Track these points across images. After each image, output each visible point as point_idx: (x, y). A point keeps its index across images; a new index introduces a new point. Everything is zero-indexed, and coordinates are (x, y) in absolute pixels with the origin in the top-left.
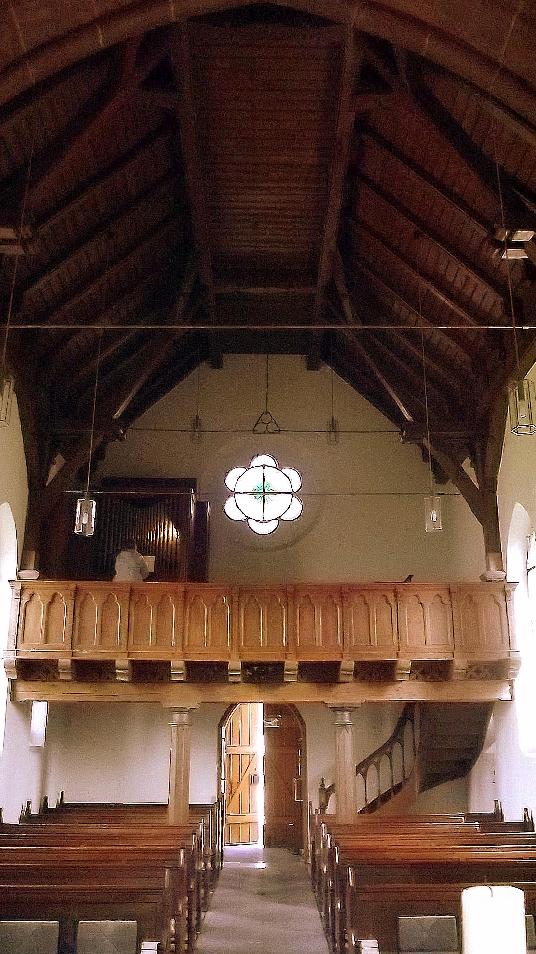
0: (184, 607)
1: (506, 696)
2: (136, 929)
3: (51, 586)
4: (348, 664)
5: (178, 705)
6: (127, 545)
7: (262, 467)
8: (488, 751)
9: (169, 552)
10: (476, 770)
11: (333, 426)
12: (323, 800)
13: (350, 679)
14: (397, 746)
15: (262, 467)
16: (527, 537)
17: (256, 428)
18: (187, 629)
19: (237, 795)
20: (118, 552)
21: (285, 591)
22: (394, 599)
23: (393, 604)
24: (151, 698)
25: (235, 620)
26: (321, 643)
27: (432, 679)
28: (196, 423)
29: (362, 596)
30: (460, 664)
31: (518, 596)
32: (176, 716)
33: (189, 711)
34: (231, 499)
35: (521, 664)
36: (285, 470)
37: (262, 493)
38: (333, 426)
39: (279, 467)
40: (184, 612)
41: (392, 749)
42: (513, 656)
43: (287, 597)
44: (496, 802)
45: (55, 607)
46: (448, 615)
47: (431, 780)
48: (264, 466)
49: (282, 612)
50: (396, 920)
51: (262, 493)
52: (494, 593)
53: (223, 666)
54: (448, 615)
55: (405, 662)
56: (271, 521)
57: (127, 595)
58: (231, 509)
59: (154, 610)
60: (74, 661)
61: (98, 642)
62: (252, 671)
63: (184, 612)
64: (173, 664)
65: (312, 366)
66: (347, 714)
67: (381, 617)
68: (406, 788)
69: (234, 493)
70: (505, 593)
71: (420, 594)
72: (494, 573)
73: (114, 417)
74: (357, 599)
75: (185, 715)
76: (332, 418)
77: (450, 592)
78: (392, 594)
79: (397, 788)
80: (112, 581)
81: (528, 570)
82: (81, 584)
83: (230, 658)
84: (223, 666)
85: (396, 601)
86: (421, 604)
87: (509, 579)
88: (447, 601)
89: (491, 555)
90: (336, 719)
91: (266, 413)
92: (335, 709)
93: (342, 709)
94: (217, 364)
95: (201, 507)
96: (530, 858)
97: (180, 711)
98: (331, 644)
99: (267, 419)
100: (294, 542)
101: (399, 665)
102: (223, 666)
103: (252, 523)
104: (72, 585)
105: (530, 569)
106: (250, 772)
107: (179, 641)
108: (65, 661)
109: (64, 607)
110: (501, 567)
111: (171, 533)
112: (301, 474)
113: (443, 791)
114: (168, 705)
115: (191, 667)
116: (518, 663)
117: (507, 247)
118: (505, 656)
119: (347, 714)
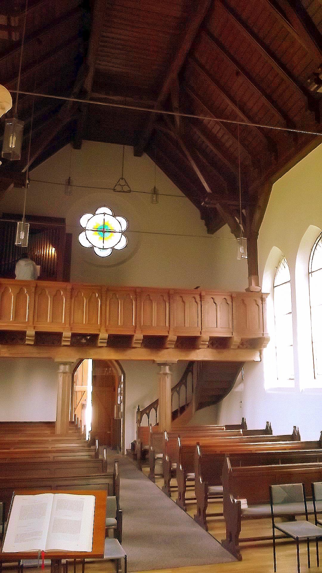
0: (71, 298)
1: (257, 359)
2: (116, 499)
4: (139, 336)
5: (64, 360)
7: (103, 215)
8: (238, 388)
9: (49, 264)
10: (225, 401)
11: (155, 192)
12: (139, 418)
13: (139, 346)
14: (183, 387)
15: (103, 215)
16: (276, 267)
18: (73, 312)
20: (17, 261)
21: (135, 292)
22: (199, 299)
23: (199, 302)
24: (46, 355)
25: (103, 307)
26: (156, 324)
27: (217, 348)
28: (69, 182)
29: (181, 297)
30: (237, 339)
31: (269, 300)
32: (62, 367)
34: (83, 234)
35: (270, 340)
36: (118, 218)
37: (103, 231)
38: (155, 192)
39: (114, 216)
40: (71, 301)
41: (180, 389)
42: (265, 336)
43: (136, 295)
44: (243, 419)
46: (230, 311)
47: (200, 406)
48: (104, 214)
49: (133, 304)
50: (313, 486)
51: (103, 231)
52: (256, 299)
53: (60, 335)
54: (230, 311)
55: (172, 337)
56: (88, 240)
57: (33, 289)
58: (82, 240)
59: (51, 300)
60: (36, 333)
61: (13, 319)
62: (86, 339)
63: (71, 301)
64: (101, 336)
65: (137, 154)
66: (167, 367)
67: (192, 309)
68: (187, 410)
69: (84, 230)
70: (263, 300)
71: (183, 295)
72: (254, 287)
73: (22, 172)
74: (178, 298)
75: (67, 367)
76: (155, 188)
78: (199, 297)
79: (182, 409)
80: (15, 279)
81: (274, 287)
83: (100, 331)
84: (60, 335)
85: (201, 301)
86: (215, 303)
87: (263, 291)
88: (230, 303)
89: (253, 277)
90: (160, 370)
92: (160, 365)
93: (165, 364)
94: (77, 146)
96: (290, 449)
97: (65, 364)
98: (162, 325)
100: (119, 264)
101: (202, 339)
102: (59, 335)
103: (96, 250)
105: (275, 287)
106: (82, 402)
107: (68, 319)
110: (258, 284)
111: (51, 251)
112: (127, 221)
113: (205, 411)
114: (57, 360)
115: (39, 335)
116: (268, 340)
117: (21, 96)
118: (261, 336)
119: (167, 368)
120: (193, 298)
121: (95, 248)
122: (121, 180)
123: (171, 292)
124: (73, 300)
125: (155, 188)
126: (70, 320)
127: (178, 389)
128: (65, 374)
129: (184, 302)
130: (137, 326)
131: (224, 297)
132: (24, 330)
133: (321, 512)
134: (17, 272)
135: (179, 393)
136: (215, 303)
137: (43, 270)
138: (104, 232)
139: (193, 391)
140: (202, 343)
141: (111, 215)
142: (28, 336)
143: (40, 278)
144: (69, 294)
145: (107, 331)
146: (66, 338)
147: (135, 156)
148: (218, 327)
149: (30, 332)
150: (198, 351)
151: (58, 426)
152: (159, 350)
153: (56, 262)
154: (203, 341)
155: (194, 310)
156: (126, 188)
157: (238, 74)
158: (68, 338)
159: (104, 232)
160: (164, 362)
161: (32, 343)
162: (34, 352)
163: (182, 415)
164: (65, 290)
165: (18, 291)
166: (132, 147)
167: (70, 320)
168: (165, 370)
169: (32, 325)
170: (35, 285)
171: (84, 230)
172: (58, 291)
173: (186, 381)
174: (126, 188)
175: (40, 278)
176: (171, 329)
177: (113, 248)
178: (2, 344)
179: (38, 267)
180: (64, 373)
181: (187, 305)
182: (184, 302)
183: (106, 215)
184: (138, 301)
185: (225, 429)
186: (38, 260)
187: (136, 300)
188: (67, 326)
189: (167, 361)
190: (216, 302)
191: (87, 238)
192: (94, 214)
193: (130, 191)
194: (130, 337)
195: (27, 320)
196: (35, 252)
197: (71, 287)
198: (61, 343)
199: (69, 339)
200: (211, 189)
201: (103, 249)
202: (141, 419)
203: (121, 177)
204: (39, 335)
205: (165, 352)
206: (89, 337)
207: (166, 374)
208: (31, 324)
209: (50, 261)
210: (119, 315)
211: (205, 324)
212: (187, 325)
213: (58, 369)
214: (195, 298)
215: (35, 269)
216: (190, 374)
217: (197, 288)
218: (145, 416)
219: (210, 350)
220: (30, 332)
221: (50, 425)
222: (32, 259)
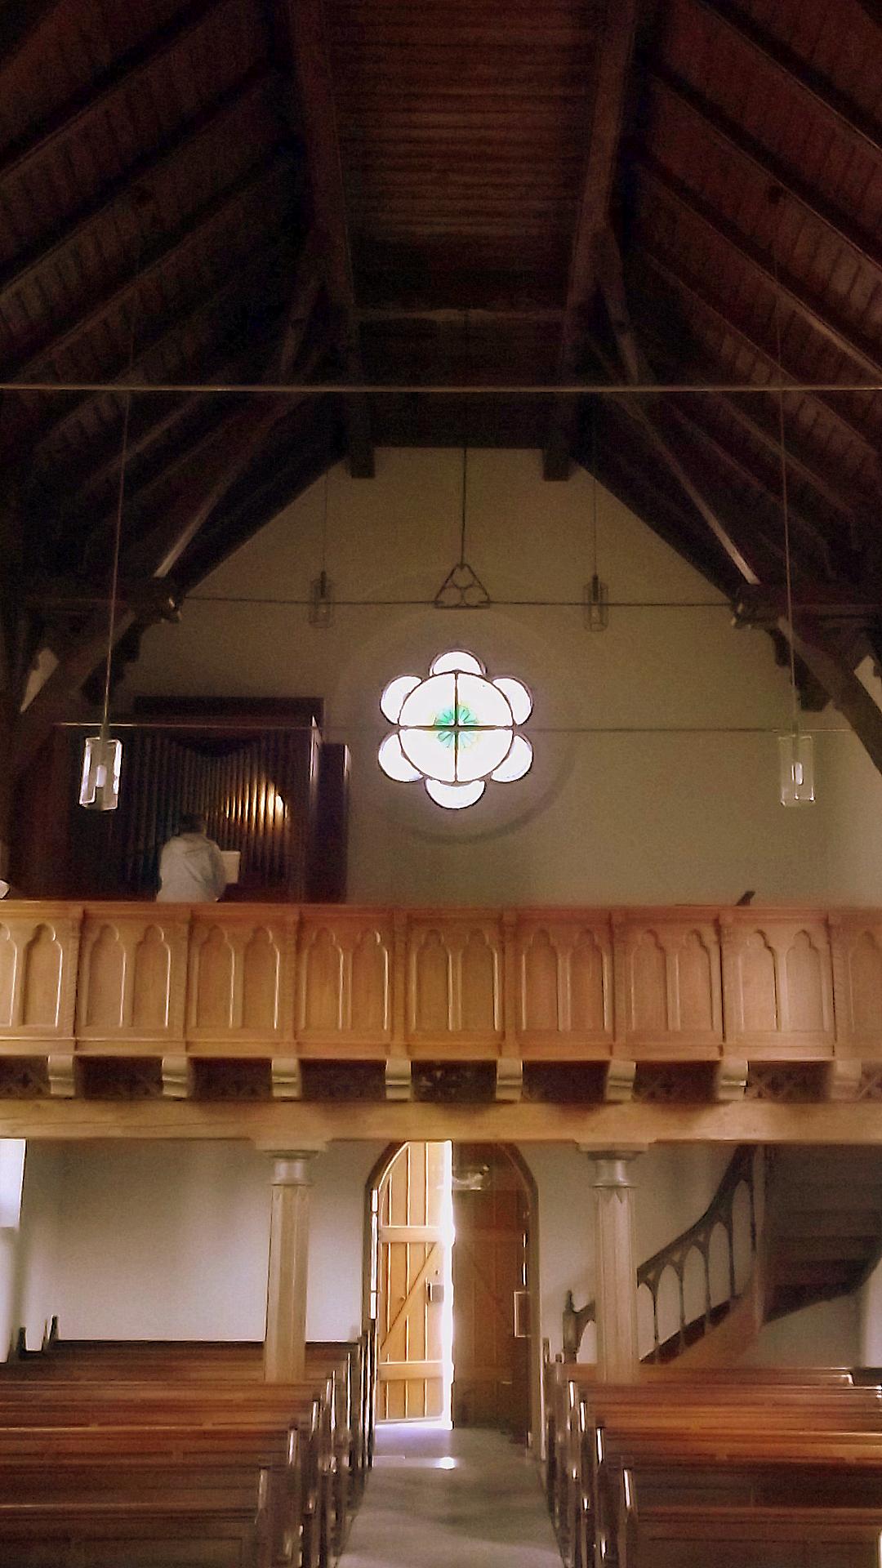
3: (32, 910)
4: (622, 1067)
5: (287, 1145)
6: (188, 825)
11: (596, 589)
12: (571, 1334)
13: (628, 1095)
14: (718, 1232)
17: (442, 598)
19: (400, 1324)
20: (165, 840)
21: (500, 921)
22: (714, 938)
24: (231, 1132)
27: (789, 1099)
28: (322, 587)
29: (650, 931)
30: (846, 1068)
32: (282, 1169)
33: (308, 1155)
38: (596, 589)
39: (488, 676)
40: (298, 960)
43: (502, 933)
45: (41, 956)
53: (264, 1065)
55: (735, 1064)
57: (185, 929)
58: (392, 760)
62: (431, 1078)
63: (298, 960)
64: (390, 1068)
65: (555, 471)
69: (395, 728)
71: (765, 929)
74: (640, 937)
75: (299, 1165)
76: (595, 578)
77: (828, 926)
79: (718, 1314)
82: (94, 907)
83: (611, 1053)
84: (264, 1065)
86: (770, 948)
88: (821, 943)
90: (597, 1174)
91: (462, 566)
93: (609, 1155)
94: (364, 470)
95: (331, 756)
97: (290, 1156)
99: (462, 578)
104: (76, 909)
107: (289, 1018)
108: (61, 1059)
109: (60, 956)
111: (273, 805)
112: (531, 690)
114: (267, 1143)
115: (201, 1066)
119: (619, 1166)
120: (695, 936)
121: (428, 781)
122: (458, 570)
123: (617, 919)
124: (305, 956)
125: (595, 578)
126: (296, 1020)
127: (701, 1238)
128: (288, 1190)
129: (662, 949)
130: (510, 1031)
131: (801, 926)
132: (158, 1054)
133: (594, 1567)
134: (164, 873)
135: (704, 1249)
136: (770, 948)
137: (249, 866)
138: (456, 728)
139: (754, 1244)
140: (725, 1083)
141: (480, 673)
142: (169, 1074)
143: (231, 894)
144: (291, 940)
145: (409, 1049)
146: (616, 1079)
147: (546, 480)
148: (783, 1029)
149: (175, 1061)
150: (722, 1110)
151: (271, 1353)
152: (590, 1109)
153: (287, 843)
154: (727, 1077)
155: (698, 972)
156: (475, 596)
157: (774, 195)
158: (626, 1080)
159: (456, 728)
160: (606, 1149)
161: (182, 1094)
162: (194, 1122)
163: (718, 1329)
164: (280, 925)
165: (138, 936)
166: (538, 451)
167: (296, 1020)
168: (612, 1174)
169: (181, 1039)
170: (188, 917)
171: (395, 728)
172: (259, 930)
173: (729, 1211)
174: (475, 596)
175: (231, 894)
176: (621, 1040)
177: (487, 780)
178: (8, 1094)
179: (231, 859)
180: (290, 1185)
181: (675, 961)
182: (662, 949)
183: (460, 675)
184: (509, 951)
185: (851, 1381)
186: (229, 835)
187: (503, 951)
188: (288, 1037)
189: (613, 1144)
190: (772, 945)
191: (403, 751)
192: (425, 676)
193: (487, 603)
194: (487, 1070)
195: (167, 1024)
196: (225, 811)
197: (296, 918)
198: (493, 1092)
199: (388, 1082)
200: (756, 573)
201: (456, 783)
202: (578, 1343)
203: (458, 561)
204: (201, 1066)
205: (609, 1112)
206: (439, 1074)
207: (615, 1188)
208: (178, 1035)
209: (269, 835)
210: (451, 1000)
211: (739, 1021)
212: (676, 1024)
213: (271, 1169)
214: (699, 936)
215: (216, 863)
216: (742, 1187)
217: (746, 899)
218: (589, 1329)
219: (765, 1106)
220: (175, 1061)
221: (258, 1345)
222: (211, 835)
